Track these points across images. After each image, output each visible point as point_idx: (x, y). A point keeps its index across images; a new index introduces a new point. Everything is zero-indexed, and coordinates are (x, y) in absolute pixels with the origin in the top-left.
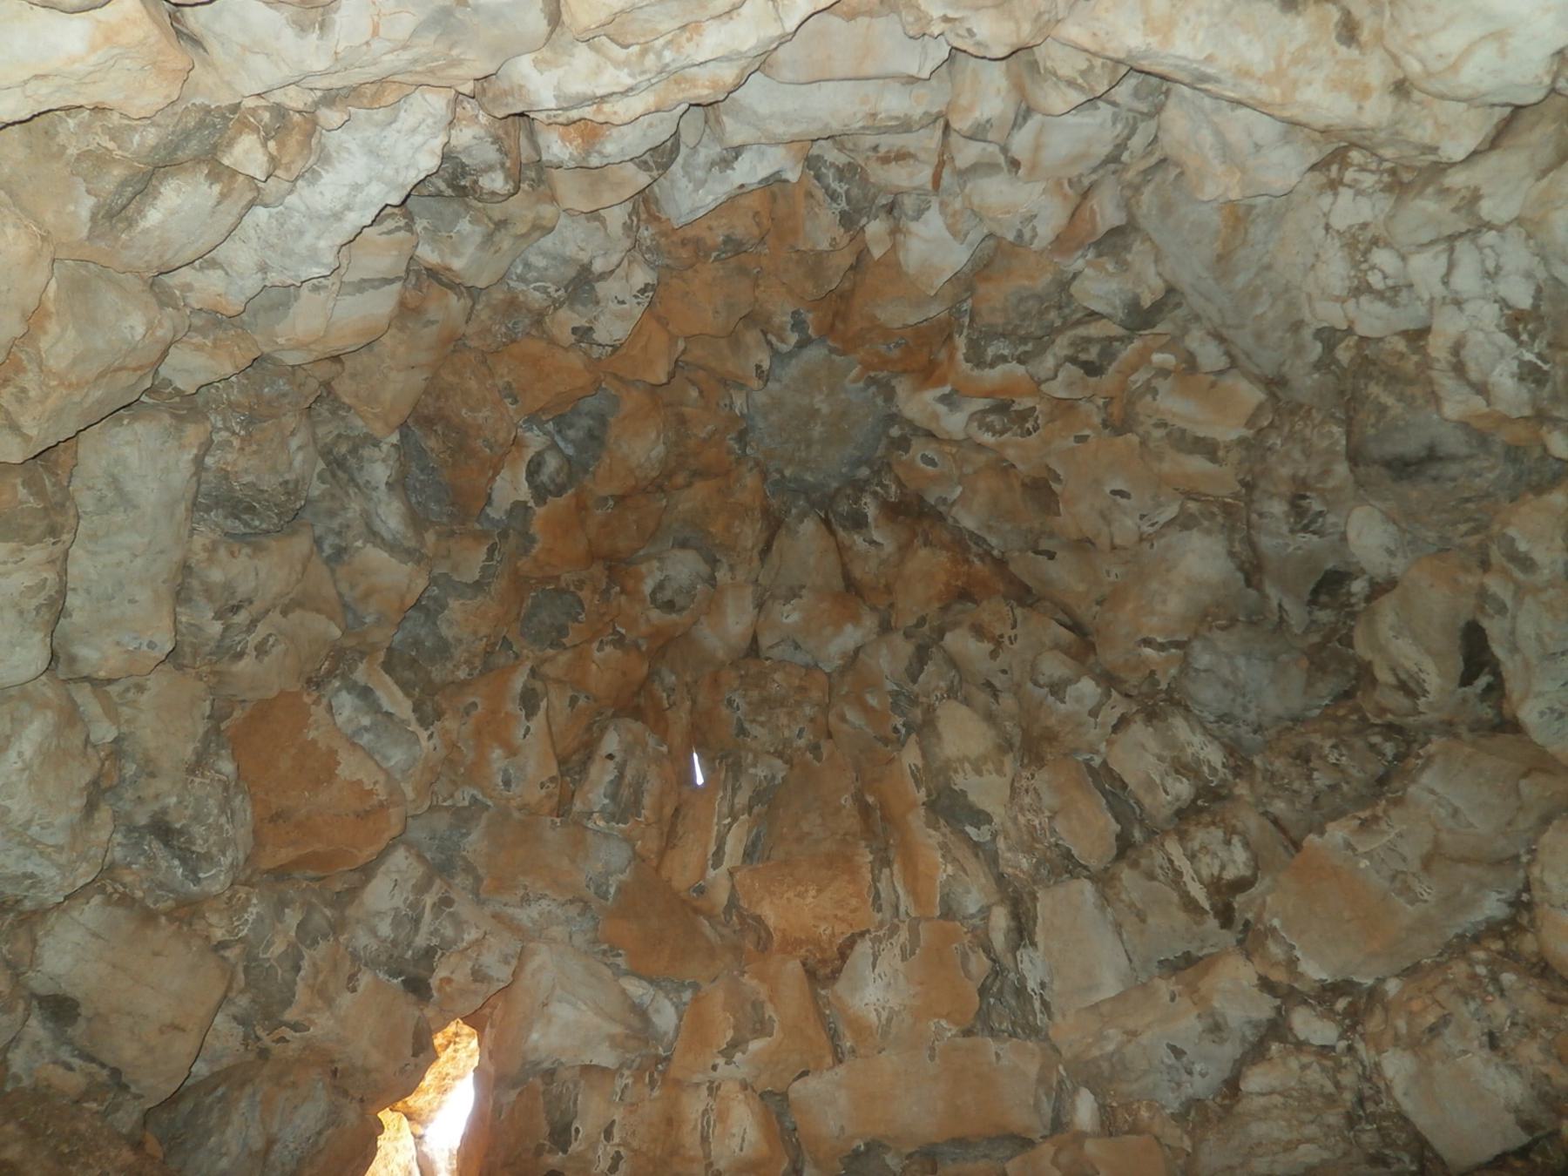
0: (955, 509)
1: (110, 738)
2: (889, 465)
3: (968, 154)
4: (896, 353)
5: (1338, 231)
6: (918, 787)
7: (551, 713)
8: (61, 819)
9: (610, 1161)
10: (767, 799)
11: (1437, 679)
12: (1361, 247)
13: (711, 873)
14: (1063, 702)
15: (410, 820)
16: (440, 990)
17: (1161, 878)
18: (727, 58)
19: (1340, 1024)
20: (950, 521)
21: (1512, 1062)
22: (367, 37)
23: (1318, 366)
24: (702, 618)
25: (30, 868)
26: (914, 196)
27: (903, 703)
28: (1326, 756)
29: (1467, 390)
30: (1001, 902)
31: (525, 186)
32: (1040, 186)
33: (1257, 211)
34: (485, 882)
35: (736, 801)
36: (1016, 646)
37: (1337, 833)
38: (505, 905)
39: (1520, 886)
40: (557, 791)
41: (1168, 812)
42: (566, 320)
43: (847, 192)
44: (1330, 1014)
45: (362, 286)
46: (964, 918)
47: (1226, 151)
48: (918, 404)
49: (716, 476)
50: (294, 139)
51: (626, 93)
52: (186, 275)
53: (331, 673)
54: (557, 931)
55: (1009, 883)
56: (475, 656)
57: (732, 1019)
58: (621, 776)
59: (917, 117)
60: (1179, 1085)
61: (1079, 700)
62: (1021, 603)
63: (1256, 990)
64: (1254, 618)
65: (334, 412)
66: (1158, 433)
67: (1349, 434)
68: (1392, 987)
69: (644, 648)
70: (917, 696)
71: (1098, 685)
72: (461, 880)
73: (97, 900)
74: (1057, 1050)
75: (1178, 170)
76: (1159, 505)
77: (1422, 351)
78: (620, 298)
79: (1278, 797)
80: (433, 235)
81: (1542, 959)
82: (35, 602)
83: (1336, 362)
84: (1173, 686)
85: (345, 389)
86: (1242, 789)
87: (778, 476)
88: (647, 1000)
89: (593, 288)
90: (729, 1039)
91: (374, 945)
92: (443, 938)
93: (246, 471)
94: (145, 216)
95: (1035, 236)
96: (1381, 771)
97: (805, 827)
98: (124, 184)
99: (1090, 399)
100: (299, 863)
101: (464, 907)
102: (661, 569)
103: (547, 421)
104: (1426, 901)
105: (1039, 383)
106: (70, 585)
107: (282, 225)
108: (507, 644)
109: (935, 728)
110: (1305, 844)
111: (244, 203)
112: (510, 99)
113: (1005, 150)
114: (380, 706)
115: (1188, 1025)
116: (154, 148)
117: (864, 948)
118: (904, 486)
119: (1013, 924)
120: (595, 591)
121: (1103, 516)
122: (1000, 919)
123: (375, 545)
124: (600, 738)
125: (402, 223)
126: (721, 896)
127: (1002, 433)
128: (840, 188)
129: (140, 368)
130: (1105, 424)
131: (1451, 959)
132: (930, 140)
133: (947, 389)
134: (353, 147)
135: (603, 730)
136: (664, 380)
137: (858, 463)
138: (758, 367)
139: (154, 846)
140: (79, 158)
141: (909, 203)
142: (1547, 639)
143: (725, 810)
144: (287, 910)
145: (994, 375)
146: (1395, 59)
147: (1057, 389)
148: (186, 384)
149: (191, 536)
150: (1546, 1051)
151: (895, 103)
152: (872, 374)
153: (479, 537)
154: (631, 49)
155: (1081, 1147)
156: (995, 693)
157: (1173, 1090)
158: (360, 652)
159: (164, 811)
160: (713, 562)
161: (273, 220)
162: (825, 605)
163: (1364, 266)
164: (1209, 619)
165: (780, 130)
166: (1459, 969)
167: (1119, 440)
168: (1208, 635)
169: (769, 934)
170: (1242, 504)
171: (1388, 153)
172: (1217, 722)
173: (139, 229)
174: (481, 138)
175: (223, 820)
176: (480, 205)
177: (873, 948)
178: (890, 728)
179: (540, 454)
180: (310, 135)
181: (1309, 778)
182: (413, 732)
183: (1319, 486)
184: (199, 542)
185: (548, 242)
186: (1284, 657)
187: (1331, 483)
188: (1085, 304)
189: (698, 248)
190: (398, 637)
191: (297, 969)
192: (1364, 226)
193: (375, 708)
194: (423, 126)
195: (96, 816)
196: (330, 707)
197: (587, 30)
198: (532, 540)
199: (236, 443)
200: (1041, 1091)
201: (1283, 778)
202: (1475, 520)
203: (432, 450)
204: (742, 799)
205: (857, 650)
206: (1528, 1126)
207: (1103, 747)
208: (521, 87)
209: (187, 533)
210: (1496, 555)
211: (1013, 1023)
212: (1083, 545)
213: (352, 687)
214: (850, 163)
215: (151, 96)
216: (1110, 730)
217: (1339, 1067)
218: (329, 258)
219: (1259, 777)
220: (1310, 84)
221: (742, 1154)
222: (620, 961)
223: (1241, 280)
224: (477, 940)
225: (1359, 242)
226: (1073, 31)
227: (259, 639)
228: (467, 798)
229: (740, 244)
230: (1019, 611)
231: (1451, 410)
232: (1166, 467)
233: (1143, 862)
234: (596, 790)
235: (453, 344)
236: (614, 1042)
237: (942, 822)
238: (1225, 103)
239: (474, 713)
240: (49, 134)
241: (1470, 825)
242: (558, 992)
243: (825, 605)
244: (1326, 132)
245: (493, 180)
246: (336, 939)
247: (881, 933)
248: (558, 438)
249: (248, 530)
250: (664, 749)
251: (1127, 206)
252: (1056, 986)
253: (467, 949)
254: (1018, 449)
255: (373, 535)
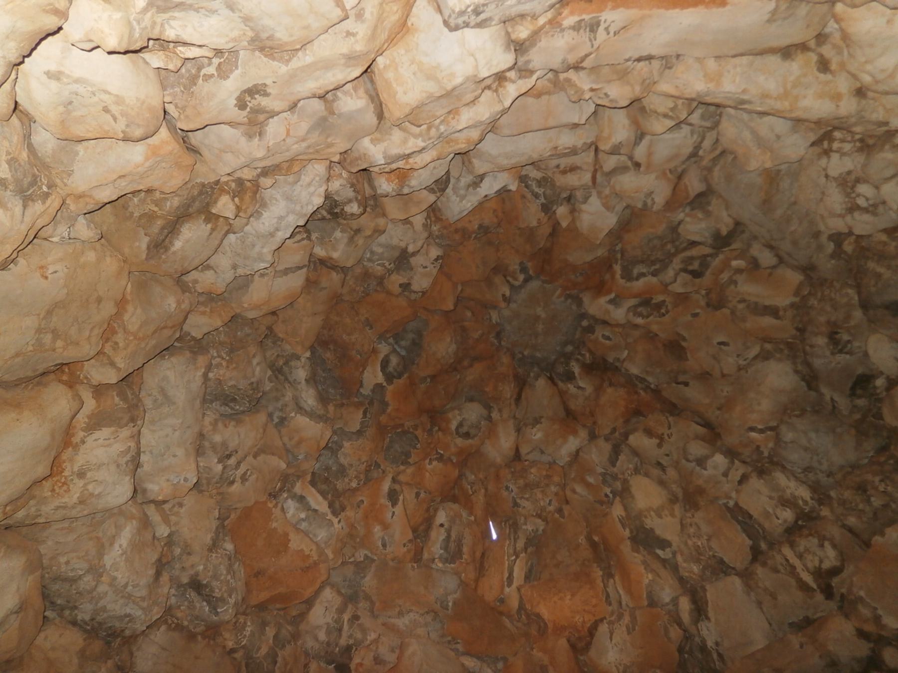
0: (625, 364)
1: (166, 535)
2: (584, 343)
3: (610, 163)
4: (580, 279)
5: (833, 178)
6: (624, 529)
8: (143, 582)
10: (535, 543)
12: (849, 184)
13: (507, 590)
14: (705, 469)
15: (331, 571)
17: (783, 571)
18: (474, 126)
20: (623, 370)
22: (284, 137)
23: (832, 256)
25: (128, 611)
26: (582, 190)
27: (609, 478)
31: (368, 209)
32: (653, 176)
33: (783, 173)
35: (517, 545)
36: (672, 439)
38: (389, 617)
40: (413, 547)
41: (780, 530)
42: (396, 280)
43: (544, 193)
45: (286, 272)
46: (663, 606)
47: (760, 142)
48: (596, 306)
50: (247, 197)
51: (420, 151)
52: (194, 275)
53: (281, 490)
58: (449, 537)
59: (579, 146)
62: (672, 414)
65: (274, 343)
66: (741, 306)
67: (859, 293)
69: (454, 461)
70: (617, 475)
71: (725, 457)
72: (363, 604)
73: (163, 628)
75: (733, 156)
78: (424, 265)
80: (321, 241)
82: (125, 459)
85: (280, 329)
86: (825, 512)
87: (521, 356)
89: (408, 262)
91: (317, 646)
93: (231, 379)
94: (174, 245)
95: (654, 203)
98: (163, 228)
99: (697, 292)
100: (272, 600)
101: (366, 620)
102: (460, 415)
103: (389, 338)
105: (666, 285)
106: (142, 450)
107: (243, 242)
108: (378, 465)
109: (630, 492)
110: (873, 542)
111: (223, 232)
112: (360, 162)
113: (631, 158)
114: (310, 506)
116: (178, 208)
117: (604, 628)
119: (693, 607)
121: (714, 357)
122: (685, 605)
123: (302, 414)
124: (435, 515)
125: (305, 236)
126: (514, 603)
127: (648, 317)
128: (540, 191)
129: (174, 326)
130: (708, 305)
132: (589, 157)
133: (613, 296)
134: (278, 197)
135: (436, 510)
136: (452, 308)
137: (566, 344)
138: (504, 295)
139: (192, 594)
140: (140, 217)
141: (579, 194)
143: (511, 551)
144: (267, 628)
145: (639, 285)
146: (855, 77)
147: (677, 288)
148: (197, 334)
149: (203, 417)
151: (567, 140)
152: (568, 292)
153: (358, 405)
154: (422, 127)
156: (663, 468)
159: (197, 574)
160: (489, 408)
161: (238, 241)
163: (853, 195)
164: (789, 412)
165: (505, 162)
167: (718, 313)
169: (545, 624)
171: (858, 129)
172: (803, 473)
173: (170, 252)
174: (344, 186)
175: (229, 577)
176: (345, 222)
177: (609, 628)
179: (387, 356)
180: (255, 193)
181: (868, 501)
182: (329, 520)
183: (846, 325)
184: (208, 420)
185: (382, 239)
186: (839, 430)
187: (852, 323)
188: (689, 238)
189: (465, 234)
190: (318, 465)
191: (276, 662)
192: (849, 173)
193: (308, 508)
194: (314, 182)
195: (161, 579)
196: (283, 509)
197: (398, 119)
198: (387, 404)
199: (224, 364)
203: (328, 359)
204: (520, 544)
205: (578, 452)
207: (734, 495)
208: (365, 154)
209: (201, 416)
212: (705, 376)
213: (294, 497)
214: (544, 177)
215: (176, 181)
216: (737, 483)
218: (269, 258)
220: (805, 97)
223: (779, 212)
224: (375, 639)
225: (847, 182)
226: (665, 87)
227: (242, 472)
228: (362, 556)
229: (488, 228)
230: (670, 419)
232: (748, 325)
233: (769, 562)
234: (436, 546)
235: (336, 300)
238: (755, 115)
239: (362, 506)
240: (125, 207)
244: (818, 123)
245: (352, 207)
246: (295, 644)
247: (613, 618)
248: (396, 347)
249: (233, 412)
250: (472, 518)
251: (706, 180)
254: (656, 324)
255: (300, 409)
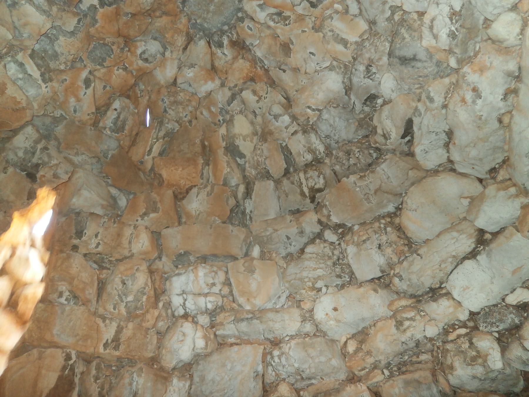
2: (235, 27)
7: (96, 90)
9: (96, 245)
11: (395, 134)
13: (146, 157)
14: (277, 122)
15: (35, 118)
16: (40, 179)
17: (296, 184)
19: (339, 236)
20: (253, 52)
21: (383, 253)
24: (158, 68)
27: (224, 112)
28: (356, 154)
29: (431, 36)
30: (243, 183)
34: (62, 145)
36: (266, 100)
37: (353, 178)
38: (69, 154)
39: (400, 203)
40: (94, 118)
44: (336, 233)
46: (230, 187)
49: (172, 15)
54: (87, 167)
55: (247, 178)
56: (68, 61)
57: (145, 206)
58: (118, 117)
60: (287, 248)
61: (283, 122)
62: (271, 86)
63: (316, 223)
64: (345, 106)
66: (330, 34)
67: (391, 46)
68: (356, 227)
69: (134, 74)
70: (229, 111)
71: (290, 118)
72: (53, 143)
74: (251, 232)
76: (324, 61)
77: (421, 20)
79: (337, 164)
81: (400, 225)
83: (393, 19)
84: (314, 123)
87: (195, 22)
88: (117, 195)
90: (143, 212)
91: (15, 159)
92: (43, 161)
96: (370, 162)
97: (182, 148)
101: (53, 152)
102: (145, 46)
104: (372, 203)
105: (294, 6)
108: (81, 59)
109: (233, 123)
114: (27, 71)
115: (293, 230)
117: (195, 190)
118: (239, 36)
119: (245, 191)
120: (118, 47)
122: (242, 189)
124: (112, 103)
126: (149, 166)
127: (277, 23)
130: (313, 28)
131: (375, 222)
137: (224, 24)
142: (430, 126)
143: (155, 136)
150: (393, 251)
153: (75, 14)
155: (253, 262)
157: (284, 249)
158: (21, 49)
160: (165, 48)
162: (203, 73)
164: (331, 103)
166: (377, 225)
167: (317, 34)
168: (329, 108)
169: (163, 181)
170: (351, 66)
172: (325, 138)
178: (217, 120)
181: (349, 160)
186: (351, 121)
200: (244, 243)
201: (341, 159)
202: (421, 84)
204: (161, 134)
206: (382, 271)
210: (424, 97)
211: (239, 222)
212: (296, 70)
213: (16, 62)
216: (291, 134)
217: (335, 249)
219: (333, 158)
221: (142, 249)
222: (109, 180)
230: (269, 89)
231: (425, 43)
232: (329, 47)
233: (291, 178)
236: (103, 206)
237: (229, 154)
239: (65, 83)
241: (392, 182)
242: (85, 186)
243: (203, 73)
247: (201, 187)
250: (136, 111)
252: (255, 213)
253: (52, 166)
254: (281, 30)
